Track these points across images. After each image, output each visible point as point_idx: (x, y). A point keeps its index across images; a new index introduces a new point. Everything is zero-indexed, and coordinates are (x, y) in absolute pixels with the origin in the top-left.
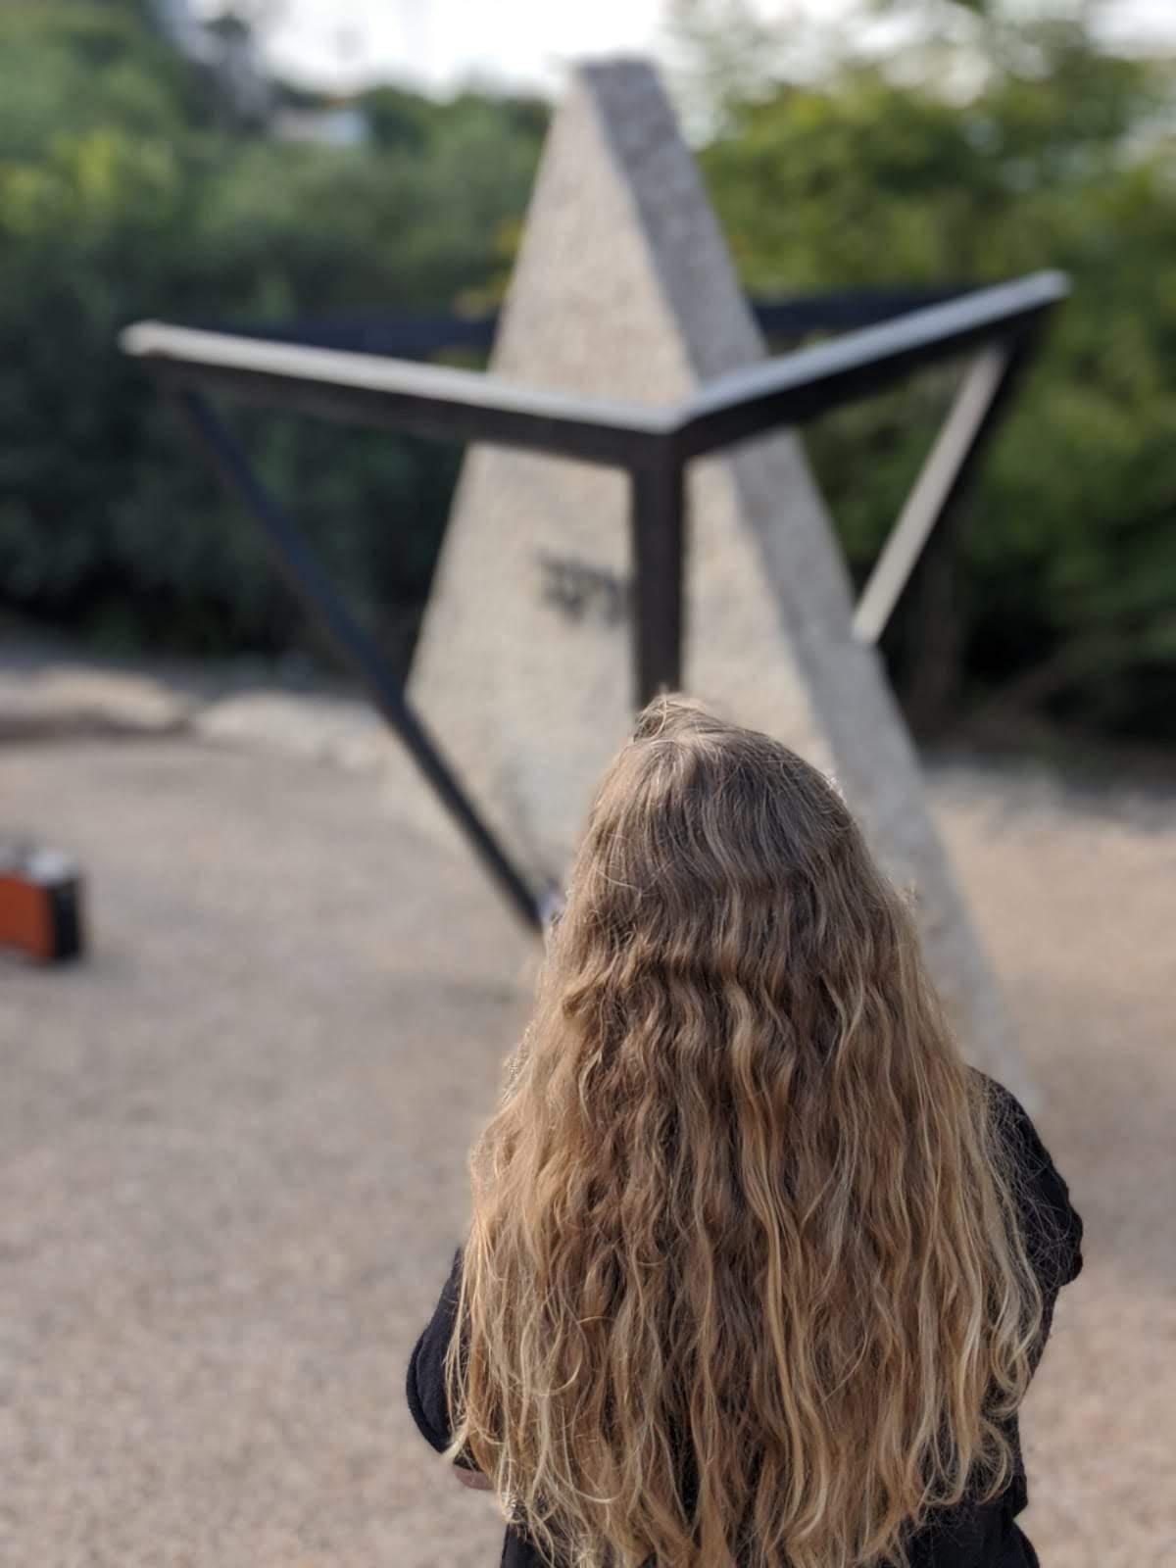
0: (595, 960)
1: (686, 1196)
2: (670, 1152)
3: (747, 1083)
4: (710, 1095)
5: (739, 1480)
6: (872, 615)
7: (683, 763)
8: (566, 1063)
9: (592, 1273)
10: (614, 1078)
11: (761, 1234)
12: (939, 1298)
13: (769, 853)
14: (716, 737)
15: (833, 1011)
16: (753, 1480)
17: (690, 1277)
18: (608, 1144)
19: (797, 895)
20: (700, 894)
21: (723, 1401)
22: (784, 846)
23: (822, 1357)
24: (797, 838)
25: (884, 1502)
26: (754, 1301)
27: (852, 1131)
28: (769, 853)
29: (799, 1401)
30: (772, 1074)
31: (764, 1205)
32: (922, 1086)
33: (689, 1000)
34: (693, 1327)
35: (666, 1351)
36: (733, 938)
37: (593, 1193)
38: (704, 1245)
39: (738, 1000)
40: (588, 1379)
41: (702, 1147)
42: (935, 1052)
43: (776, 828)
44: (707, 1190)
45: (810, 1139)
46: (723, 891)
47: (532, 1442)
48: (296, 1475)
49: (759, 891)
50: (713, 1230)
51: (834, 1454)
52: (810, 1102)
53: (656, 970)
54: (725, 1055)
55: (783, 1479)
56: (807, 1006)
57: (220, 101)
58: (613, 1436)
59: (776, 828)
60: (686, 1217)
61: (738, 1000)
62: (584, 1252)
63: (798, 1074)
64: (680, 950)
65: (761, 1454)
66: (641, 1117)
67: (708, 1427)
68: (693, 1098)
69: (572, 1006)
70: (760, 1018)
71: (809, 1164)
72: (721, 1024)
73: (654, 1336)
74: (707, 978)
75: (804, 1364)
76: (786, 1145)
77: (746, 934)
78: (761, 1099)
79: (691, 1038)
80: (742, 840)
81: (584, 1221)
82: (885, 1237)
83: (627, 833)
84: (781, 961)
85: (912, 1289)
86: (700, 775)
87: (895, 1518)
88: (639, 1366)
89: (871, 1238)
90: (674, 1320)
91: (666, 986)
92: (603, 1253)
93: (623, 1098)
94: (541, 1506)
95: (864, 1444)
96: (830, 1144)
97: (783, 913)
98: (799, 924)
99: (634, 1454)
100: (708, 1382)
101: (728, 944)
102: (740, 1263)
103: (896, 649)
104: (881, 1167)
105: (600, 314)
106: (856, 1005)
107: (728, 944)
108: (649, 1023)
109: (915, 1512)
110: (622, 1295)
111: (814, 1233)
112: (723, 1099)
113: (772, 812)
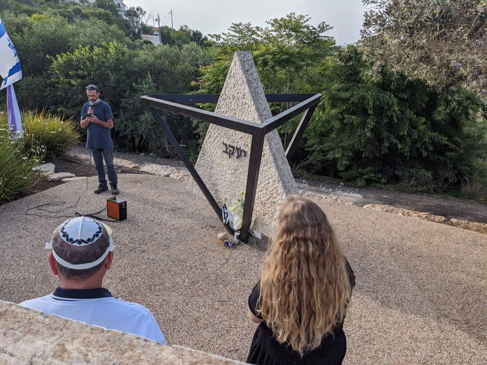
0: (285, 237)
1: (302, 275)
2: (299, 268)
3: (311, 257)
4: (305, 258)
5: (308, 319)
6: (286, 153)
7: (300, 206)
8: (280, 253)
9: (286, 287)
10: (289, 256)
11: (313, 280)
12: (338, 290)
13: (314, 220)
14: (304, 201)
15: (324, 244)
16: (310, 319)
17: (302, 287)
18: (288, 266)
19: (319, 227)
20: (304, 227)
21: (307, 307)
22: (316, 219)
23: (322, 300)
24: (318, 218)
25: (329, 323)
26: (312, 291)
27: (327, 264)
28: (314, 220)
29: (318, 306)
30: (315, 255)
31: (314, 275)
32: (337, 256)
33: (302, 243)
34: (303, 295)
35: (298, 299)
36: (309, 234)
37: (286, 274)
38: (304, 281)
39: (310, 244)
40: (285, 303)
41: (304, 267)
42: (338, 251)
43: (315, 216)
44: (305, 272)
45: (320, 265)
46: (308, 226)
47: (275, 313)
48: (185, 322)
49: (313, 226)
50: (306, 279)
51: (323, 314)
52: (321, 259)
53: (297, 239)
54: (308, 252)
55: (315, 318)
56: (321, 244)
57: (130, 27)
58: (289, 313)
59: (315, 216)
60: (302, 277)
61: (310, 244)
62: (284, 284)
63: (319, 255)
64: (301, 235)
65: (312, 314)
66: (294, 261)
67: (305, 311)
68: (303, 259)
69: (281, 244)
70: (313, 247)
71: (321, 269)
72: (307, 247)
73: (297, 297)
74: (305, 240)
75: (319, 300)
76: (317, 266)
77: (311, 233)
78: (313, 259)
79: (303, 249)
80: (310, 218)
81: (284, 279)
82: (331, 280)
83: (291, 217)
84: (317, 237)
85: (335, 289)
86: (303, 207)
87: (331, 325)
88: (294, 301)
89: (330, 282)
90: (300, 294)
91: (298, 241)
92: (288, 283)
93: (291, 259)
94: (275, 323)
95: (327, 313)
96: (324, 266)
97: (317, 230)
98: (319, 231)
99: (292, 315)
100: (305, 303)
101: (309, 234)
102: (310, 285)
103: (288, 157)
104: (331, 269)
105: (240, 98)
106: (328, 244)
107: (309, 234)
108: (295, 247)
109: (335, 324)
110: (291, 290)
111: (321, 280)
112: (307, 259)
113: (315, 214)
